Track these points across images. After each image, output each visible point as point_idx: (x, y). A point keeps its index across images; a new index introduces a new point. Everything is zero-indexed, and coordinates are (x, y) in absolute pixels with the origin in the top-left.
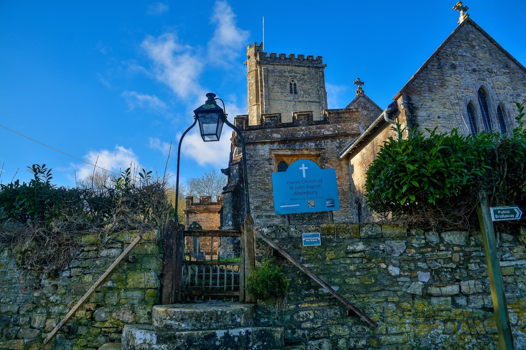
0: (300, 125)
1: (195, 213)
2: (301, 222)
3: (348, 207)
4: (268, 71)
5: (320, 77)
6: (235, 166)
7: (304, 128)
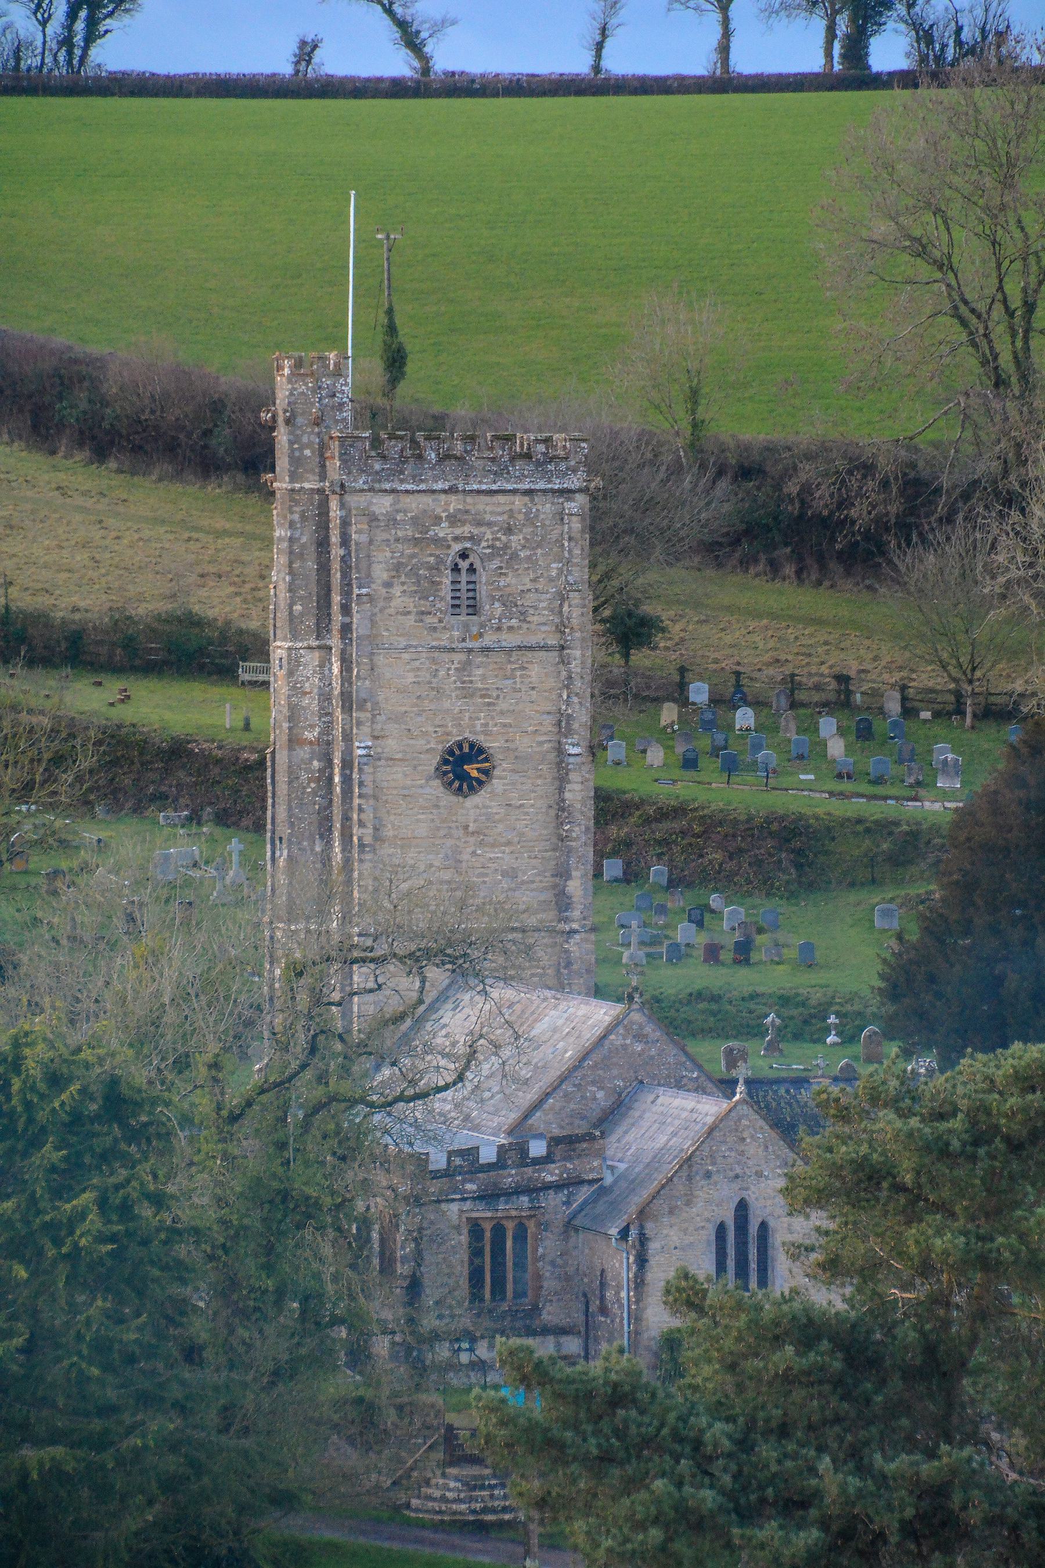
5: (570, 539)
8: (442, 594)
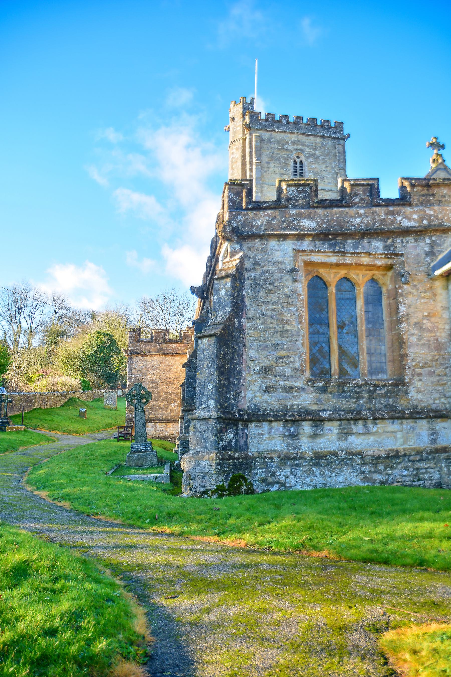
0: (355, 204)
1: (143, 355)
2: (355, 403)
3: (445, 375)
4: (261, 140)
5: (339, 153)
6: (223, 281)
7: (362, 211)
8: (290, 168)
